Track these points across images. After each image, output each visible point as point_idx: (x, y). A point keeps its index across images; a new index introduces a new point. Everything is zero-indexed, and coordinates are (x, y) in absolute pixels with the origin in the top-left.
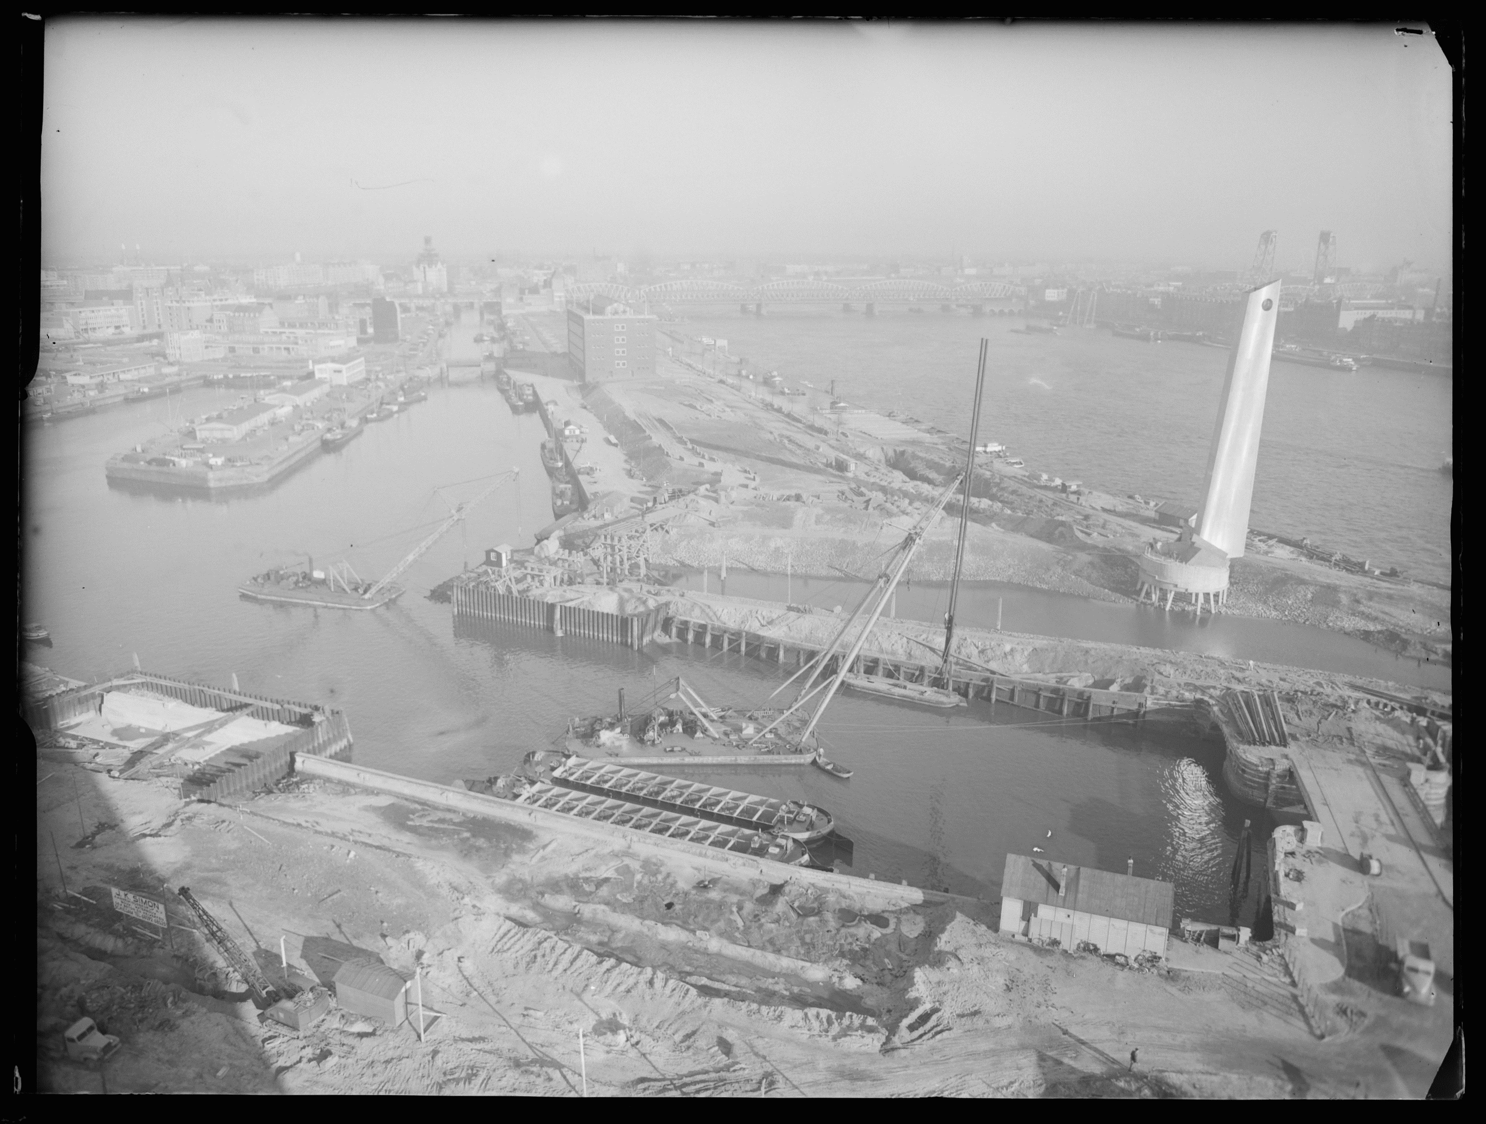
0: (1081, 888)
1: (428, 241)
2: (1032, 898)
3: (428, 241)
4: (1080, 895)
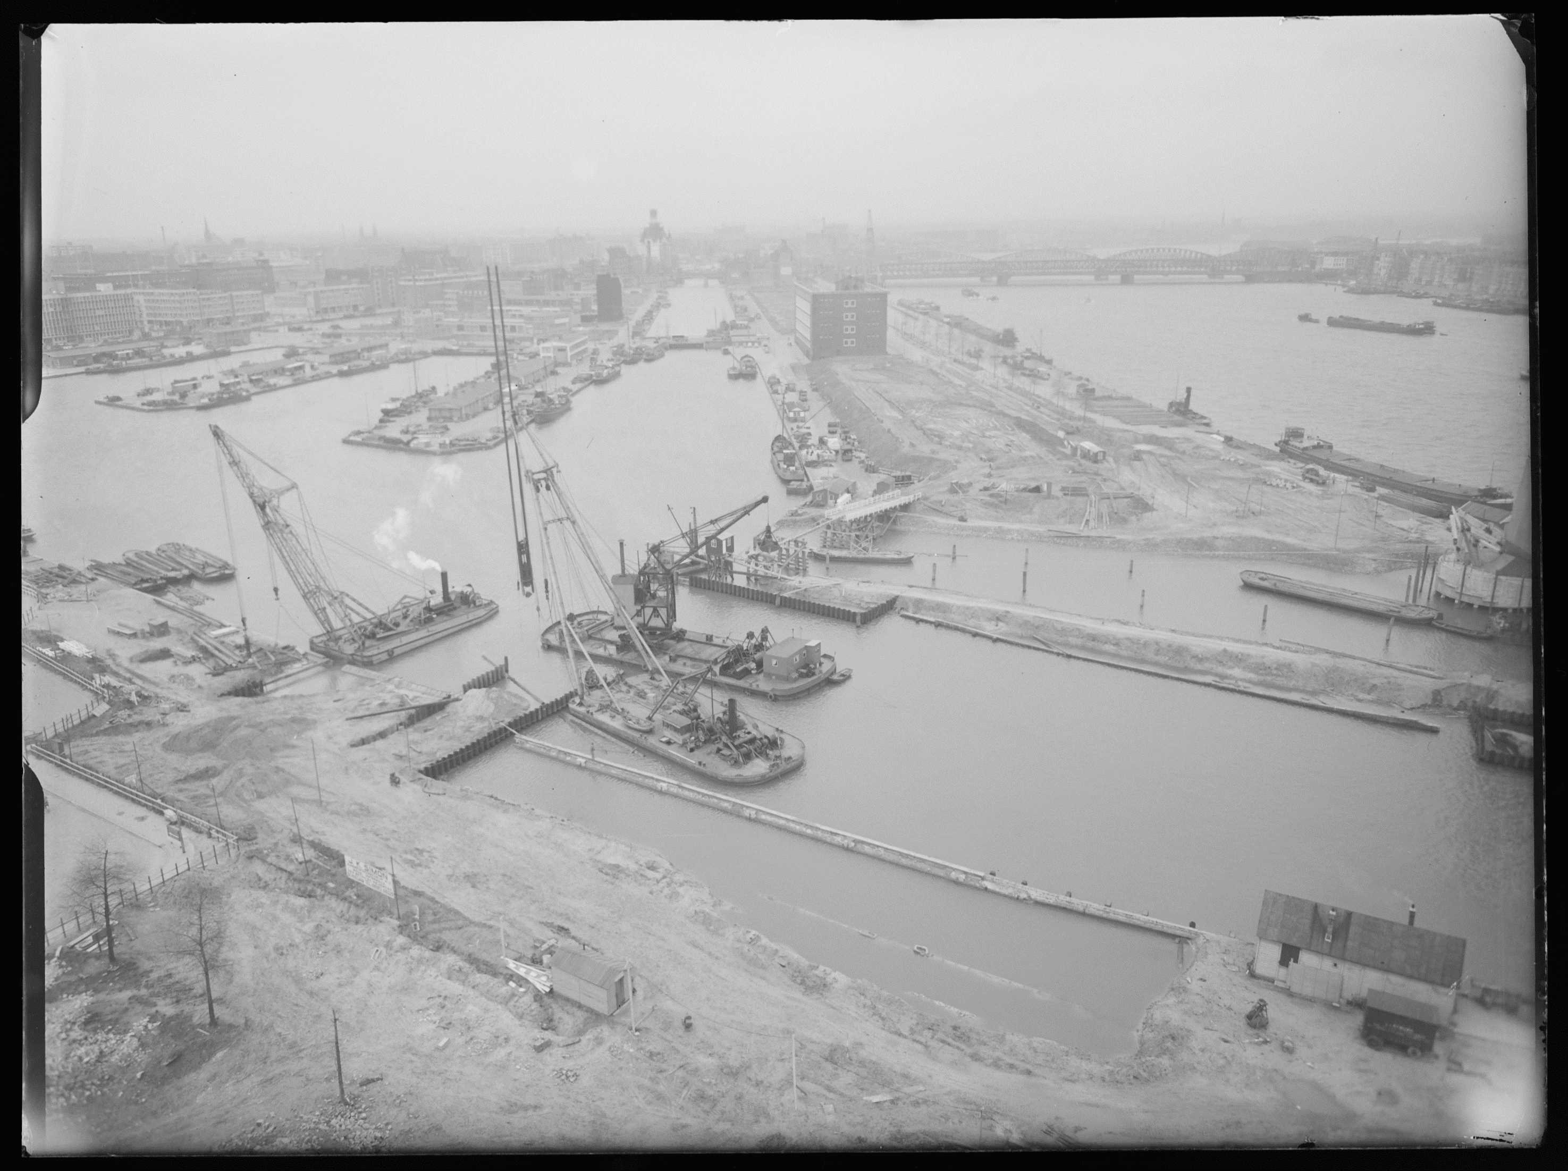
0: (1351, 935)
1: (654, 213)
2: (1294, 941)
3: (654, 213)
4: (1350, 944)
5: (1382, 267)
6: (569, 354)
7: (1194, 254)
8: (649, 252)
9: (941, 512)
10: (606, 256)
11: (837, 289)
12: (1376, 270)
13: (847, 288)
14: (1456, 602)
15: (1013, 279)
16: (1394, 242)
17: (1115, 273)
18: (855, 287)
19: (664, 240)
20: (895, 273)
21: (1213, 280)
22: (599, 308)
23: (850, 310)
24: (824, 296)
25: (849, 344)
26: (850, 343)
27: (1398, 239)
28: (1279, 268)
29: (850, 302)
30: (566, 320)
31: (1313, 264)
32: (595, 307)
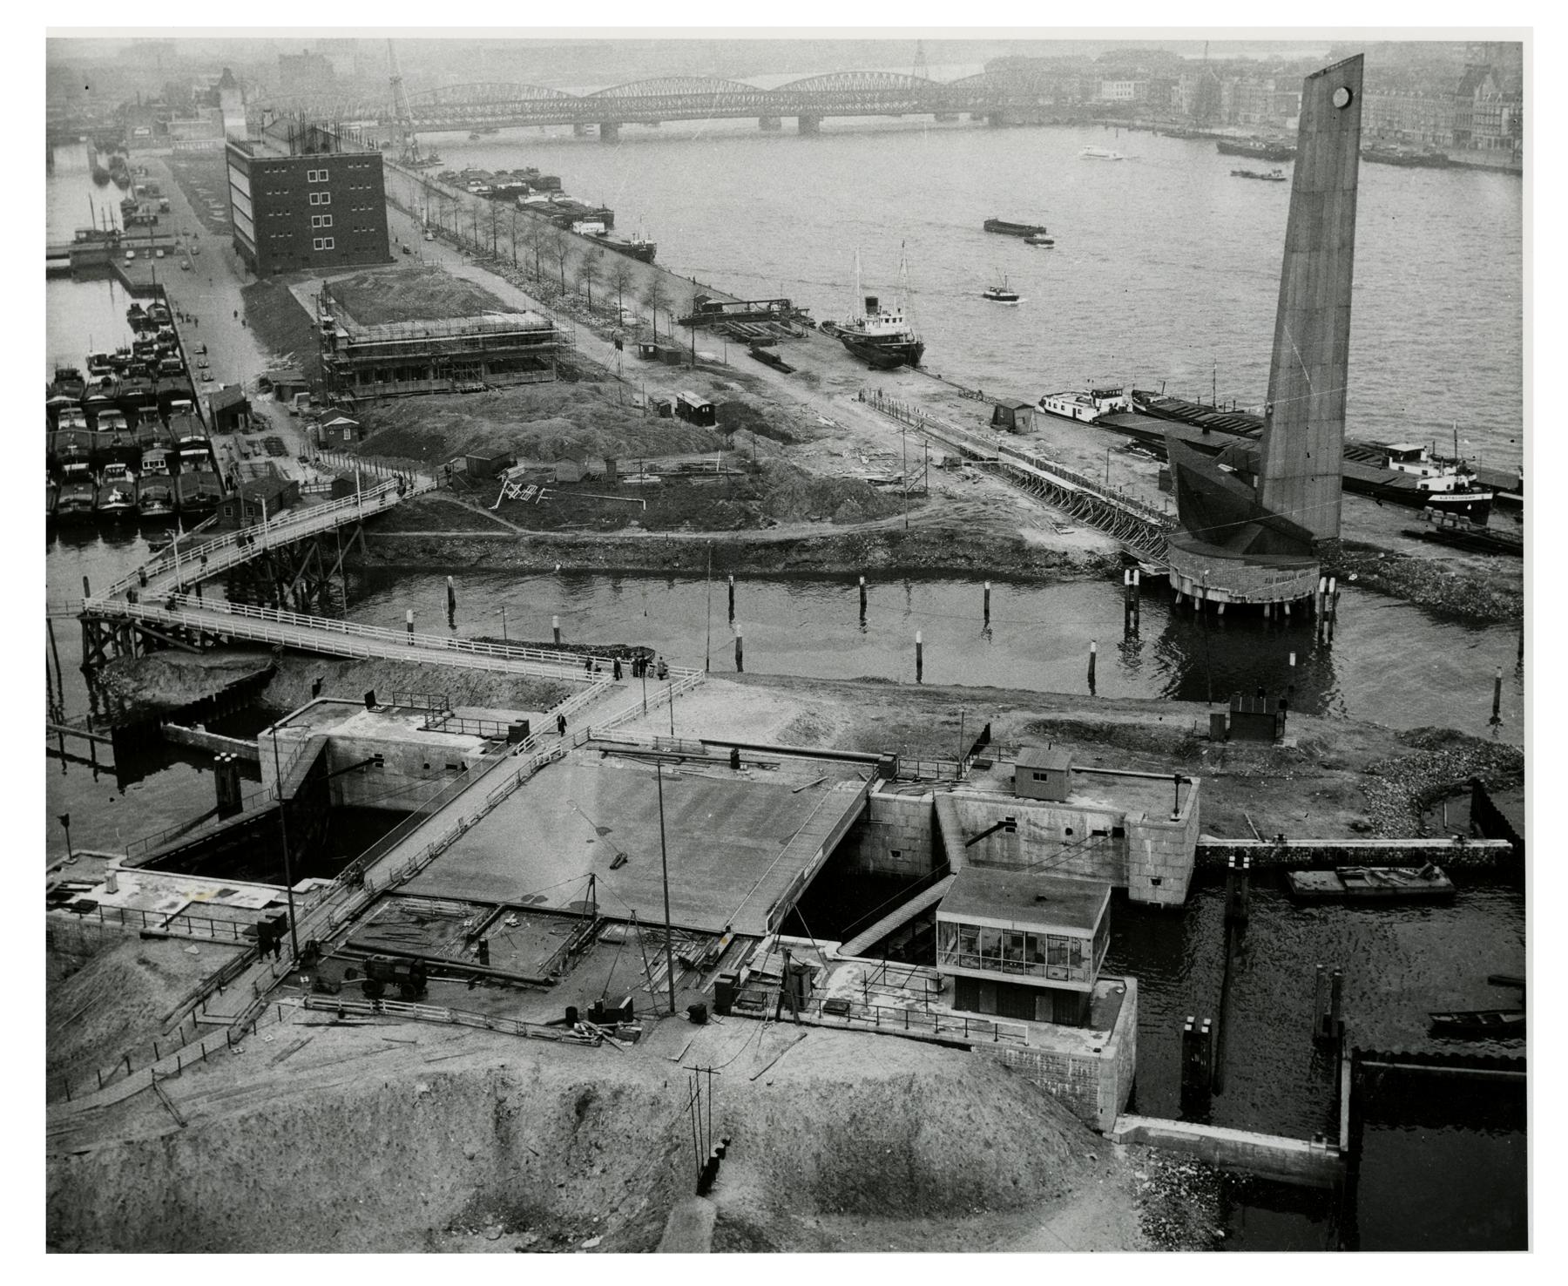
5: (1183, 95)
7: (901, 78)
9: (820, 1026)
11: (293, 151)
12: (1175, 100)
13: (310, 150)
14: (732, 578)
15: (827, 123)
16: (1200, 56)
17: (792, 114)
18: (325, 147)
20: (438, 122)
21: (942, 125)
22: (1181, 508)
24: (273, 164)
26: (324, 245)
27: (1206, 53)
28: (1041, 101)
29: (317, 172)
31: (1086, 94)
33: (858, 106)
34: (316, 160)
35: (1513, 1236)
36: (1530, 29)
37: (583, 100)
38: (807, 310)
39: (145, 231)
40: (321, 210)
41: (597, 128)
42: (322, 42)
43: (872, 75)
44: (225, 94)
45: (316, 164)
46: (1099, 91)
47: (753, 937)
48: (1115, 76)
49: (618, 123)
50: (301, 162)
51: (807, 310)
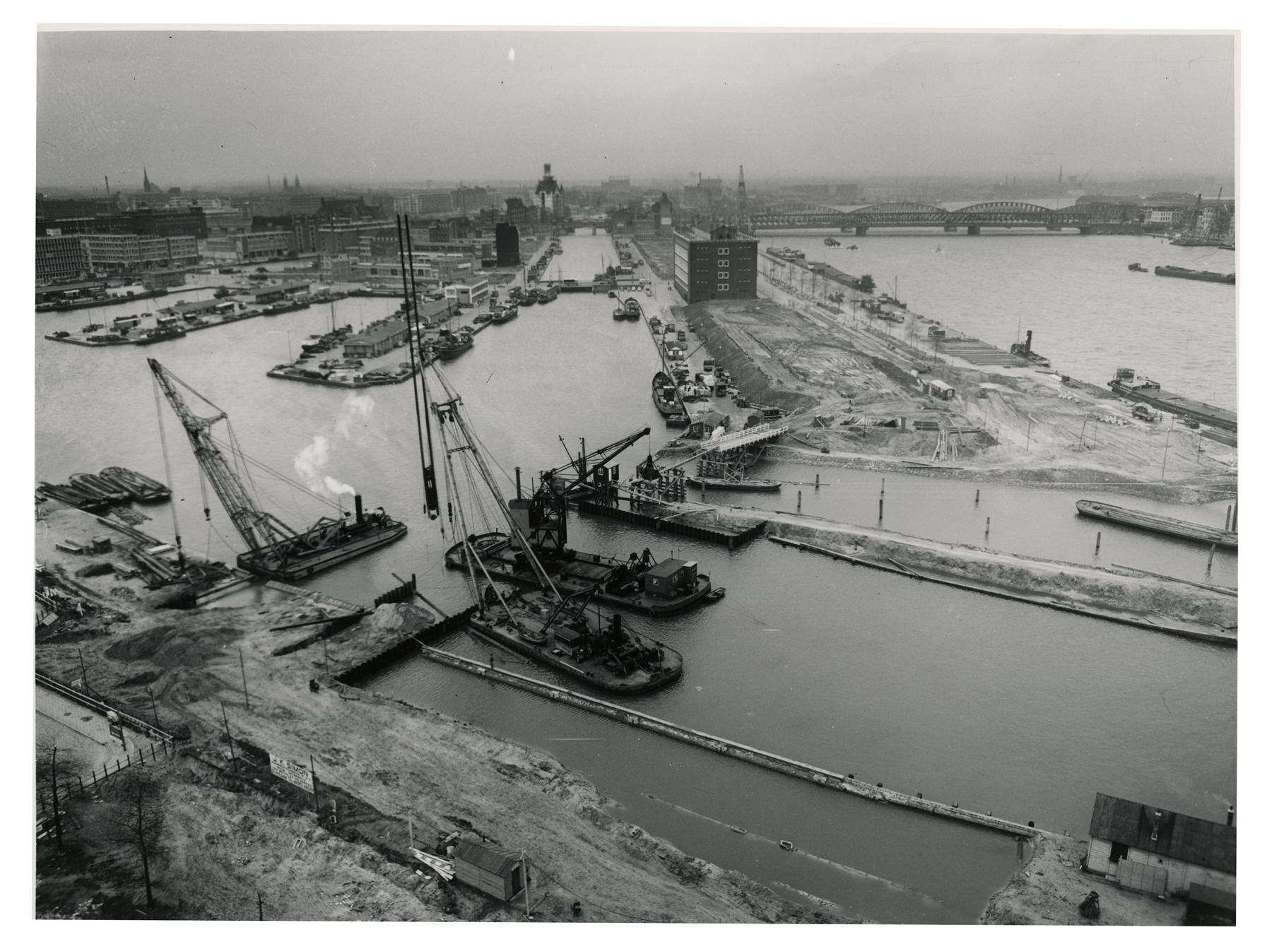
1: (547, 168)
6: (471, 296)
8: (543, 203)
10: (505, 207)
11: (712, 238)
12: (1199, 224)
13: (721, 237)
16: (1216, 198)
18: (729, 236)
19: (557, 192)
23: (724, 257)
25: (723, 289)
28: (1111, 222)
29: (723, 250)
30: (468, 265)
32: (494, 253)
33: (998, 222)
34: (723, 243)
35: (1233, 923)
36: (1239, 32)
37: (849, 214)
38: (461, 404)
39: (629, 277)
40: (724, 269)
41: (854, 229)
42: (799, 188)
43: (1012, 204)
44: (662, 206)
45: (723, 245)
46: (1150, 217)
47: (489, 897)
48: (1161, 209)
49: (867, 228)
50: (715, 243)
51: (461, 404)
